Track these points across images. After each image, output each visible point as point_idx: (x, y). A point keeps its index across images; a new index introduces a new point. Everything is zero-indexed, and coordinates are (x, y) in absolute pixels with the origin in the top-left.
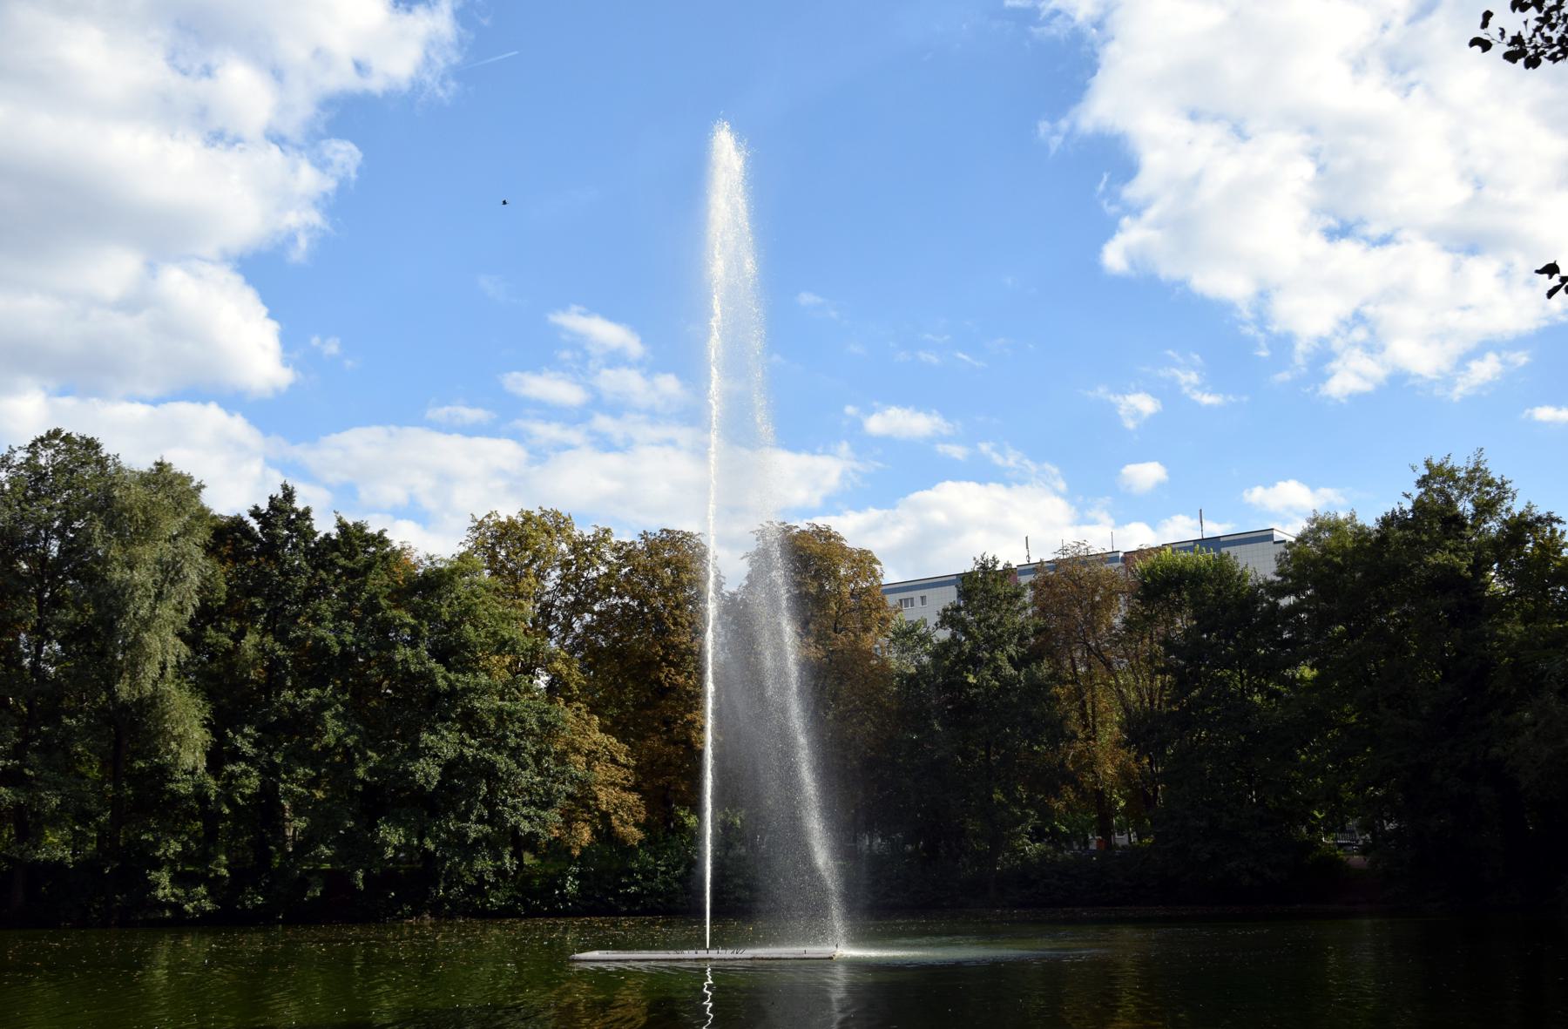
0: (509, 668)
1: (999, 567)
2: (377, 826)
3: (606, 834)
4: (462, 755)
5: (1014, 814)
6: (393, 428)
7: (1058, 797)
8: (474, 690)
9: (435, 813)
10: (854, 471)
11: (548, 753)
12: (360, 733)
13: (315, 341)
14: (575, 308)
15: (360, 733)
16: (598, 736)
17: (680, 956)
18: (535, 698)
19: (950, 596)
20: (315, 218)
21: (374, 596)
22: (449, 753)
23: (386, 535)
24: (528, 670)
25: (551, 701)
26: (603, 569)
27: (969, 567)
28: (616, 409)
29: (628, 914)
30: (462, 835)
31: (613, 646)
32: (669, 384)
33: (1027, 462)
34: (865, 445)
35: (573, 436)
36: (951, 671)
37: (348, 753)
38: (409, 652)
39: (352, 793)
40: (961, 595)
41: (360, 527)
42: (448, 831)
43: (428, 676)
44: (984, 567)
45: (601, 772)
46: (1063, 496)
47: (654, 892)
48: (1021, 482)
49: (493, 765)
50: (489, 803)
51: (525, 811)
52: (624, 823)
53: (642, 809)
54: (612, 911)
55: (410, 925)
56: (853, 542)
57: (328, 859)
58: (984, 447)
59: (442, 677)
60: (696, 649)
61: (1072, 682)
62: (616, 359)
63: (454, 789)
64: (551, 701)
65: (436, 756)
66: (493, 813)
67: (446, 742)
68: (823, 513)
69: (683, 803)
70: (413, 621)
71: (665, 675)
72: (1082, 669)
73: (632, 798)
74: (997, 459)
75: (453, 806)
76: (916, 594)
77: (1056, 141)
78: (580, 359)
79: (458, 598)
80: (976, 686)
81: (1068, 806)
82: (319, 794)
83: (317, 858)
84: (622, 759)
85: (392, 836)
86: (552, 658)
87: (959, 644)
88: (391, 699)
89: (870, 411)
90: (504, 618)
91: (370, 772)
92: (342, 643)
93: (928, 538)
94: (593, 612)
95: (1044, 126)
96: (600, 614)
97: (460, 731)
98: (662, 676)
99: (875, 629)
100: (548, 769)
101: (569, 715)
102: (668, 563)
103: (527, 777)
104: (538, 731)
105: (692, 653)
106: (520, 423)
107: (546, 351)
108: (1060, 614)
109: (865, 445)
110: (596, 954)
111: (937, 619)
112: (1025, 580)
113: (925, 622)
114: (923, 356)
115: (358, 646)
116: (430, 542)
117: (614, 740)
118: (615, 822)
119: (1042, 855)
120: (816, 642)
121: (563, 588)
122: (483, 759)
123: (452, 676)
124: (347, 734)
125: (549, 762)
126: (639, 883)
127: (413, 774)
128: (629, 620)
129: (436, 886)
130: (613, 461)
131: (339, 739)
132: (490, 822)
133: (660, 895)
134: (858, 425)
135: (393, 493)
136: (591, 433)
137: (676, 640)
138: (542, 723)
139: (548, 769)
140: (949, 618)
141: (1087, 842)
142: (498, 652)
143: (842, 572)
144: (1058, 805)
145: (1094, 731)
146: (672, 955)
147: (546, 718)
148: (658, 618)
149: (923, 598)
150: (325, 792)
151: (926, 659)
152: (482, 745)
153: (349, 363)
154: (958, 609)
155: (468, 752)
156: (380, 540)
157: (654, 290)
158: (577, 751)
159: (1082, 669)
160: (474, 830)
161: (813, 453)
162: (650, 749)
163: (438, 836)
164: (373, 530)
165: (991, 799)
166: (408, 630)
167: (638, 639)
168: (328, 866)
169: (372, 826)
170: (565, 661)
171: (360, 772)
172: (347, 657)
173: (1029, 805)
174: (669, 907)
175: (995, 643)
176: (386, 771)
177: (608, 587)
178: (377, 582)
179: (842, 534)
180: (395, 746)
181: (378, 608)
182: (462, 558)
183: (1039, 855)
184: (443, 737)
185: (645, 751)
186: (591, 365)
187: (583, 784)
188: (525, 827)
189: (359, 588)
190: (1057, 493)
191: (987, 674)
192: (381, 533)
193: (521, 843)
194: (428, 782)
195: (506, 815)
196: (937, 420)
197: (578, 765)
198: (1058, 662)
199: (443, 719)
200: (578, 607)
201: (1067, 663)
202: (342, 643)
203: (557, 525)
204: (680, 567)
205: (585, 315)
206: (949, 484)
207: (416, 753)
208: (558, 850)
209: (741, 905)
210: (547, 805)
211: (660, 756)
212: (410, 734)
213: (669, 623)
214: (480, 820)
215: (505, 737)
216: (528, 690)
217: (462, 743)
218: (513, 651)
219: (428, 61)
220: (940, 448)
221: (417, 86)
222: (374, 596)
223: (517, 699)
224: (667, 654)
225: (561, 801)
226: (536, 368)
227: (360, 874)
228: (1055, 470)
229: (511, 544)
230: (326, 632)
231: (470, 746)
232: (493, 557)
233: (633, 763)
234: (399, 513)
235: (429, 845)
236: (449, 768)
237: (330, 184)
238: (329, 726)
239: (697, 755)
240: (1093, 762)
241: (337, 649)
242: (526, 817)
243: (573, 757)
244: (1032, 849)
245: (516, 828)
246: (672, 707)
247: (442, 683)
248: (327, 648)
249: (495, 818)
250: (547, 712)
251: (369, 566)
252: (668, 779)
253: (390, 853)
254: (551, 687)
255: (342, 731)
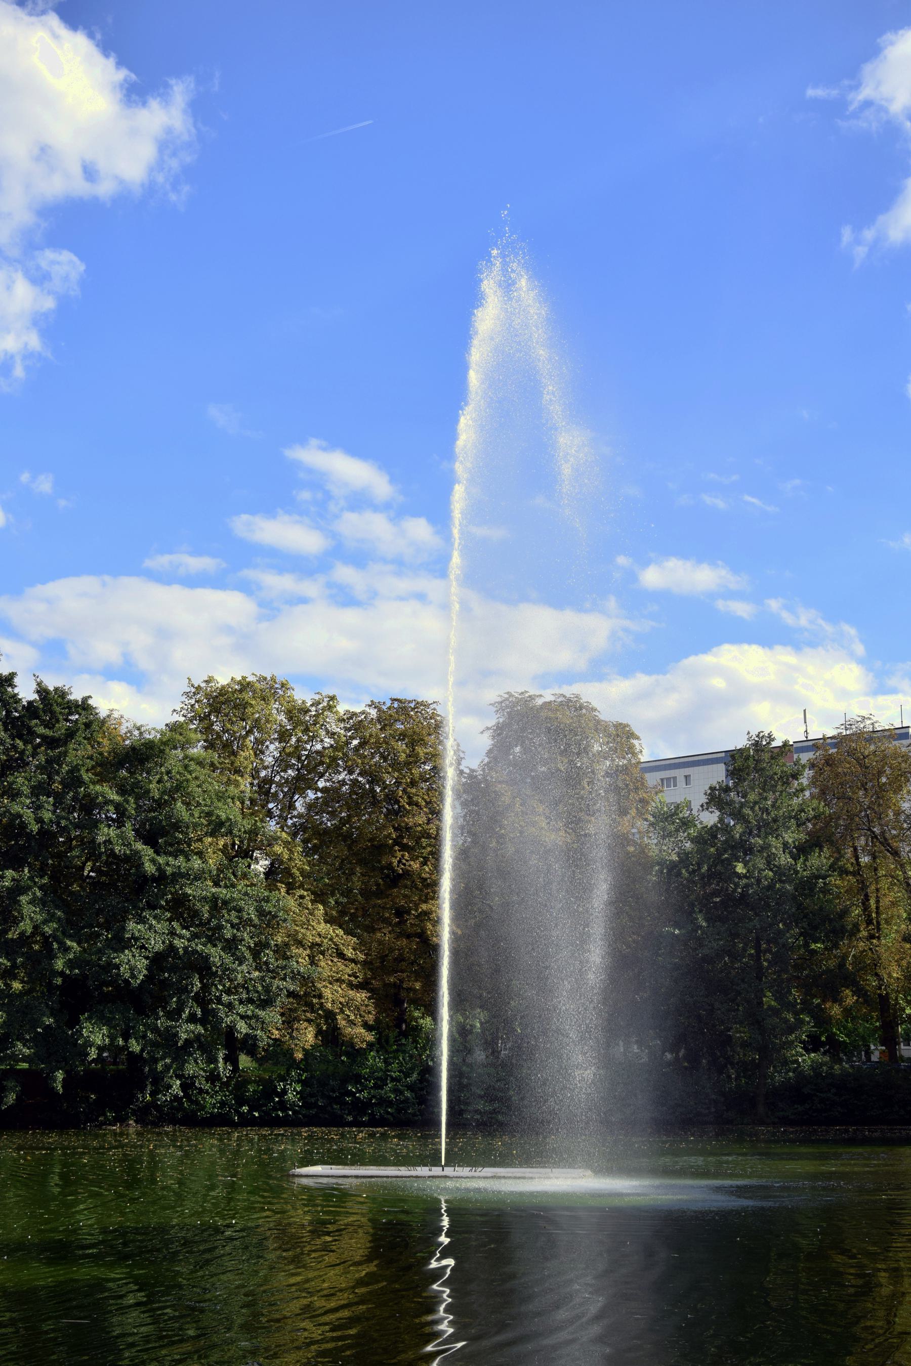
0: (224, 850)
1: (777, 743)
2: (78, 1022)
3: (330, 1036)
4: (172, 948)
5: (786, 1021)
6: (107, 578)
7: (837, 999)
8: (186, 875)
9: (143, 1010)
10: (626, 630)
11: (267, 945)
12: (59, 920)
13: (25, 477)
14: (314, 442)
15: (59, 920)
16: (323, 927)
17: (413, 1173)
18: (252, 885)
19: (718, 775)
20: (34, 341)
21: (75, 769)
22: (156, 944)
23: (90, 702)
24: (246, 854)
25: (271, 887)
26: (328, 741)
27: (741, 742)
28: (360, 558)
29: (357, 1124)
30: (170, 1037)
31: (337, 828)
32: (420, 529)
33: (821, 622)
34: (636, 600)
35: (310, 588)
36: (718, 859)
37: (46, 941)
38: (113, 832)
39: (50, 986)
40: (730, 774)
41: (61, 693)
42: (155, 1030)
43: (134, 859)
44: (757, 744)
45: (326, 966)
46: (860, 661)
47: (384, 1102)
48: (813, 645)
49: (206, 958)
50: (202, 1000)
51: (241, 1010)
52: (352, 1023)
53: (371, 1008)
54: (336, 1122)
55: (115, 1134)
56: (607, 714)
57: (25, 1059)
58: (774, 604)
59: (150, 861)
60: (433, 832)
61: (854, 874)
62: (360, 501)
63: (164, 984)
64: (271, 887)
65: (143, 947)
66: (205, 1011)
67: (153, 932)
68: (583, 678)
69: (416, 1003)
70: (116, 797)
71: (398, 860)
72: (865, 860)
73: (361, 996)
74: (787, 618)
75: (162, 1002)
76: (680, 773)
77: (861, 252)
78: (319, 502)
79: (168, 772)
80: (745, 876)
81: (847, 1012)
82: (17, 985)
83: (14, 1058)
84: (349, 953)
85: (95, 1035)
86: (272, 840)
87: (727, 829)
88: (95, 884)
89: (646, 563)
90: (221, 796)
91: (70, 964)
92: (39, 820)
93: (706, 706)
94: (317, 790)
95: (847, 234)
96: (324, 790)
97: (170, 920)
98: (395, 862)
99: (633, 812)
100: (266, 963)
101: (291, 903)
102: (403, 736)
103: (245, 971)
104: (256, 921)
105: (429, 836)
106: (249, 574)
107: (282, 491)
108: (842, 797)
109: (636, 600)
110: (318, 1169)
111: (704, 799)
112: (805, 757)
113: (688, 805)
114: (708, 499)
115: (58, 824)
116: (139, 709)
117: (340, 932)
118: (341, 1022)
119: (816, 1067)
120: (566, 825)
121: (282, 762)
122: (195, 952)
123: (161, 860)
124: (45, 922)
125: (268, 956)
126: (367, 1091)
127: (117, 967)
128: (359, 799)
129: (143, 1090)
130: (350, 617)
131: (36, 927)
132: (203, 1022)
133: (390, 1103)
134: (631, 577)
135: (106, 650)
136: (329, 585)
137: (410, 821)
138: (261, 913)
139: (266, 963)
140: (716, 798)
141: (868, 1053)
142: (212, 834)
143: (596, 748)
144: (836, 1010)
145: (879, 929)
146: (403, 1171)
147: (267, 907)
148: (391, 798)
149: (687, 777)
150: (22, 982)
151: (688, 845)
152: (195, 936)
153: (62, 503)
154: (727, 790)
155: (177, 943)
156: (84, 706)
157: (407, 420)
158: (300, 943)
159: (865, 860)
160: (185, 1031)
161: (581, 609)
162: (380, 942)
163: (144, 1037)
164: (76, 696)
165: (761, 1003)
166: (111, 808)
167: (373, 822)
168: (25, 1065)
169: (74, 1022)
170: (286, 844)
171: (59, 964)
172: (46, 835)
173: (802, 1011)
174: (403, 1115)
175: (769, 827)
176: (88, 963)
177: (334, 759)
178: (78, 753)
179: (595, 704)
180: (98, 935)
181: (80, 782)
182: (174, 728)
183: (812, 1068)
184: (151, 927)
185: (375, 944)
186: (332, 507)
187: (306, 980)
188: (242, 1028)
189: (58, 760)
190: (852, 656)
191: (760, 863)
192: (85, 699)
193: (235, 1045)
194: (133, 976)
195: (221, 1014)
196: (723, 572)
197: (300, 959)
198: (838, 851)
199: (152, 906)
200: (300, 784)
201: (849, 851)
202: (39, 820)
203: (270, 690)
204: (414, 740)
205: (324, 449)
206: (726, 647)
207: (121, 943)
208: (278, 1054)
209: (494, 1116)
210: (265, 1004)
211: (392, 950)
212: (116, 921)
213: (404, 802)
214: (192, 1019)
215: (220, 927)
216: (245, 876)
217: (172, 933)
218: (230, 832)
219: (159, 165)
220: (720, 605)
221: (150, 189)
222: (75, 769)
223: (233, 886)
224: (402, 837)
225: (282, 1000)
226: (270, 512)
227: (60, 1075)
228: (852, 631)
229: (224, 710)
230: (22, 808)
231: (181, 937)
232: (208, 729)
233: (361, 957)
234: (110, 673)
235: (135, 1047)
236: (157, 961)
237: (49, 303)
238: (25, 911)
239: (431, 950)
240: (876, 963)
241: (35, 828)
242: (242, 1017)
243: (295, 950)
244: (807, 1060)
245: (231, 1029)
246: (405, 896)
247: (149, 868)
248: (23, 826)
249: (208, 1018)
250: (267, 900)
251: (71, 734)
252: (399, 979)
253: (93, 1054)
254: (270, 873)
255: (39, 918)
